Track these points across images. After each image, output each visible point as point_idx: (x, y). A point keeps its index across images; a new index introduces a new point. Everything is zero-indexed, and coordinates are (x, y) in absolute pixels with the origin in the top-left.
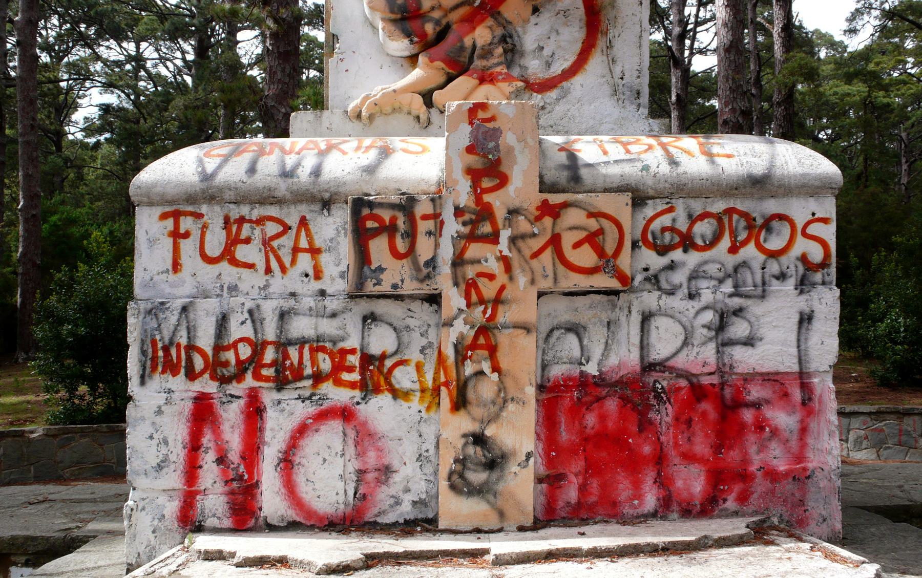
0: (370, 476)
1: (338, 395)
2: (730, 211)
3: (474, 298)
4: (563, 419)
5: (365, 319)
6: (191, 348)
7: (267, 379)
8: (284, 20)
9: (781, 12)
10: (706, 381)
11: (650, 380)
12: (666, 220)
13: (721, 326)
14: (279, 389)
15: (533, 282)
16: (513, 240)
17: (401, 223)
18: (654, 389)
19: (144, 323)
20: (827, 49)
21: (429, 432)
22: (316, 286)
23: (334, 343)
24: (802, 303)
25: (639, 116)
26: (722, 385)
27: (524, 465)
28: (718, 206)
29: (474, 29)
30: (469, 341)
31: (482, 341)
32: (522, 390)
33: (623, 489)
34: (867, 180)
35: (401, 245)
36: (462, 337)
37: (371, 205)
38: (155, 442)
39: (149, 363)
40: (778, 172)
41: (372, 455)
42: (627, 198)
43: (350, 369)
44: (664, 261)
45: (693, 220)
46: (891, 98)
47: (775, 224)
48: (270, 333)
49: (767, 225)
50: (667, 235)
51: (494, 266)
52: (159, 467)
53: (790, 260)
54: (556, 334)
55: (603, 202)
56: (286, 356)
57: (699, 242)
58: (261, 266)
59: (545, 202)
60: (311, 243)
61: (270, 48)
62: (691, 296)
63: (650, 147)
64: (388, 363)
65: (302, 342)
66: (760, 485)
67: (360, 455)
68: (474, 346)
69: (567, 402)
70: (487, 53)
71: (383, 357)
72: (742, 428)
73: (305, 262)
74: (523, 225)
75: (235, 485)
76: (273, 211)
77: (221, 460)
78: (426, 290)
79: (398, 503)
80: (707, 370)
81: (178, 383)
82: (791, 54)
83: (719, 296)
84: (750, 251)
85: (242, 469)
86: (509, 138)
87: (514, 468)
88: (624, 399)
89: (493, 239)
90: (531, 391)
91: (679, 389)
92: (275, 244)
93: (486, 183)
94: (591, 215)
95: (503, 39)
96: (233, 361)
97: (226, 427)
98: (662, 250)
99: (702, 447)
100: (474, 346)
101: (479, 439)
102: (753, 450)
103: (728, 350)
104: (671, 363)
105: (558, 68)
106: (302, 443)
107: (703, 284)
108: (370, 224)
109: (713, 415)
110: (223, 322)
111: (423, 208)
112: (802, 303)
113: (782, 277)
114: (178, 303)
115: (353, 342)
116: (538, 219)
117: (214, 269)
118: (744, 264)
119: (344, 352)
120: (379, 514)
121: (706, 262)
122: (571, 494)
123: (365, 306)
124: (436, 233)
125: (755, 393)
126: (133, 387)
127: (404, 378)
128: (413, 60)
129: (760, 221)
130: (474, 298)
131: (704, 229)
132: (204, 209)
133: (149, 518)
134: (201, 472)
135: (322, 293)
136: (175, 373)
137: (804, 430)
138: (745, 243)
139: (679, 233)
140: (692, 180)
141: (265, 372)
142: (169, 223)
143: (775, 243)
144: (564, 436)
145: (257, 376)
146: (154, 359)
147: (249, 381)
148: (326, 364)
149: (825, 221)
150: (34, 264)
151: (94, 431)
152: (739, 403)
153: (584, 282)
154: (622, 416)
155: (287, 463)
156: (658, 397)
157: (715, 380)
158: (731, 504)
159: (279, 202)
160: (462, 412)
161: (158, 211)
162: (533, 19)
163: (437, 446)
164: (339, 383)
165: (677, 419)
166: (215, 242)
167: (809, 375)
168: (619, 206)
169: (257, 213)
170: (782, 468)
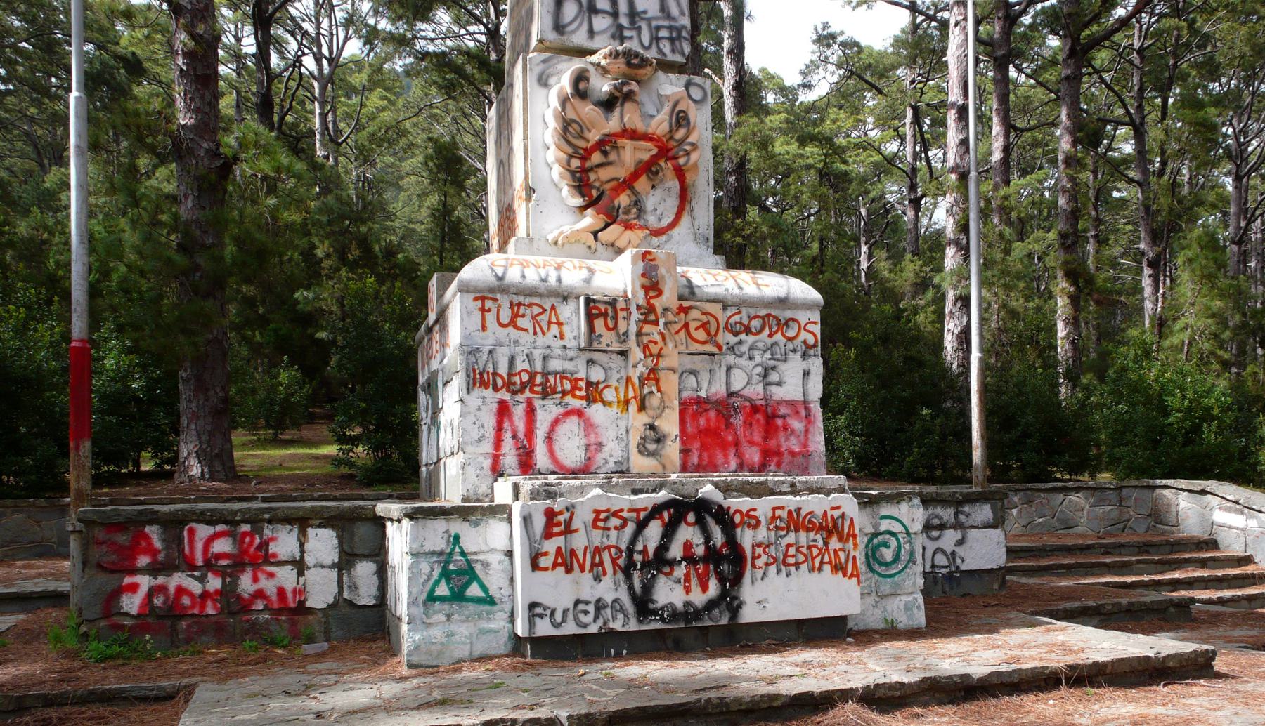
0: (593, 448)
2: (768, 315)
3: (648, 353)
4: (688, 420)
5: (588, 362)
6: (495, 374)
7: (537, 393)
8: (201, 36)
9: (733, 66)
10: (759, 403)
11: (731, 401)
12: (737, 318)
13: (765, 376)
14: (543, 399)
15: (676, 346)
16: (666, 324)
17: (610, 311)
18: (733, 406)
19: (467, 359)
20: (776, 94)
21: (622, 424)
22: (561, 343)
23: (572, 374)
24: (804, 365)
26: (767, 405)
27: (674, 441)
28: (763, 312)
29: (619, 195)
30: (645, 376)
31: (652, 376)
32: (672, 402)
33: (719, 458)
34: (822, 265)
35: (611, 324)
36: (642, 374)
37: (594, 301)
38: (476, 426)
39: (471, 382)
40: (792, 296)
41: (592, 436)
42: (720, 305)
43: (580, 389)
44: (736, 339)
45: (751, 318)
46: (848, 165)
47: (791, 323)
48: (539, 368)
49: (787, 323)
50: (738, 326)
51: (657, 337)
52: (479, 440)
54: (685, 375)
55: (709, 307)
56: (548, 381)
57: (754, 331)
58: (531, 330)
59: (681, 305)
60: (557, 319)
61: (184, 68)
62: (750, 359)
63: (727, 278)
64: (601, 386)
65: (556, 373)
66: (787, 459)
67: (587, 436)
68: (648, 379)
69: (690, 412)
71: (598, 383)
72: (777, 427)
73: (555, 329)
74: (670, 317)
75: (522, 450)
76: (536, 300)
77: (514, 437)
78: (623, 348)
79: (607, 462)
80: (759, 397)
81: (489, 393)
82: (744, 117)
83: (764, 359)
84: (778, 337)
85: (525, 442)
87: (669, 443)
88: (719, 412)
89: (656, 323)
90: (676, 403)
91: (746, 407)
92: (538, 318)
93: (652, 294)
94: (704, 313)
95: (637, 203)
96: (519, 382)
97: (516, 418)
98: (736, 334)
99: (757, 437)
100: (648, 379)
101: (652, 427)
102: (782, 440)
103: (769, 387)
104: (741, 393)
106: (557, 428)
107: (756, 352)
108: (594, 311)
109: (762, 421)
110: (512, 360)
111: (621, 305)
112: (804, 365)
113: (794, 351)
114: (487, 349)
115: (582, 374)
116: (678, 314)
117: (506, 331)
118: (775, 343)
119: (577, 380)
120: (597, 468)
121: (757, 341)
122: (694, 459)
123: (588, 355)
124: (628, 318)
127: (609, 395)
128: (583, 209)
129: (783, 321)
130: (648, 353)
131: (756, 324)
132: (498, 296)
133: (473, 469)
134: (503, 444)
135: (565, 347)
136: (487, 388)
137: (807, 431)
138: (776, 332)
139: (744, 325)
140: (750, 298)
141: (536, 389)
142: (479, 303)
143: (791, 333)
144: (689, 429)
145: (532, 391)
146: (475, 379)
147: (527, 394)
148: (568, 386)
149: (815, 323)
151: (30, 506)
153: (701, 348)
154: (717, 420)
155: (549, 439)
156: (735, 410)
157: (763, 403)
158: (773, 467)
159: (540, 295)
160: (643, 413)
161: (472, 296)
162: (652, 192)
163: (627, 431)
164: (574, 396)
165: (745, 422)
166: (505, 316)
167: (809, 403)
168: (715, 309)
169: (528, 301)
170: (797, 449)
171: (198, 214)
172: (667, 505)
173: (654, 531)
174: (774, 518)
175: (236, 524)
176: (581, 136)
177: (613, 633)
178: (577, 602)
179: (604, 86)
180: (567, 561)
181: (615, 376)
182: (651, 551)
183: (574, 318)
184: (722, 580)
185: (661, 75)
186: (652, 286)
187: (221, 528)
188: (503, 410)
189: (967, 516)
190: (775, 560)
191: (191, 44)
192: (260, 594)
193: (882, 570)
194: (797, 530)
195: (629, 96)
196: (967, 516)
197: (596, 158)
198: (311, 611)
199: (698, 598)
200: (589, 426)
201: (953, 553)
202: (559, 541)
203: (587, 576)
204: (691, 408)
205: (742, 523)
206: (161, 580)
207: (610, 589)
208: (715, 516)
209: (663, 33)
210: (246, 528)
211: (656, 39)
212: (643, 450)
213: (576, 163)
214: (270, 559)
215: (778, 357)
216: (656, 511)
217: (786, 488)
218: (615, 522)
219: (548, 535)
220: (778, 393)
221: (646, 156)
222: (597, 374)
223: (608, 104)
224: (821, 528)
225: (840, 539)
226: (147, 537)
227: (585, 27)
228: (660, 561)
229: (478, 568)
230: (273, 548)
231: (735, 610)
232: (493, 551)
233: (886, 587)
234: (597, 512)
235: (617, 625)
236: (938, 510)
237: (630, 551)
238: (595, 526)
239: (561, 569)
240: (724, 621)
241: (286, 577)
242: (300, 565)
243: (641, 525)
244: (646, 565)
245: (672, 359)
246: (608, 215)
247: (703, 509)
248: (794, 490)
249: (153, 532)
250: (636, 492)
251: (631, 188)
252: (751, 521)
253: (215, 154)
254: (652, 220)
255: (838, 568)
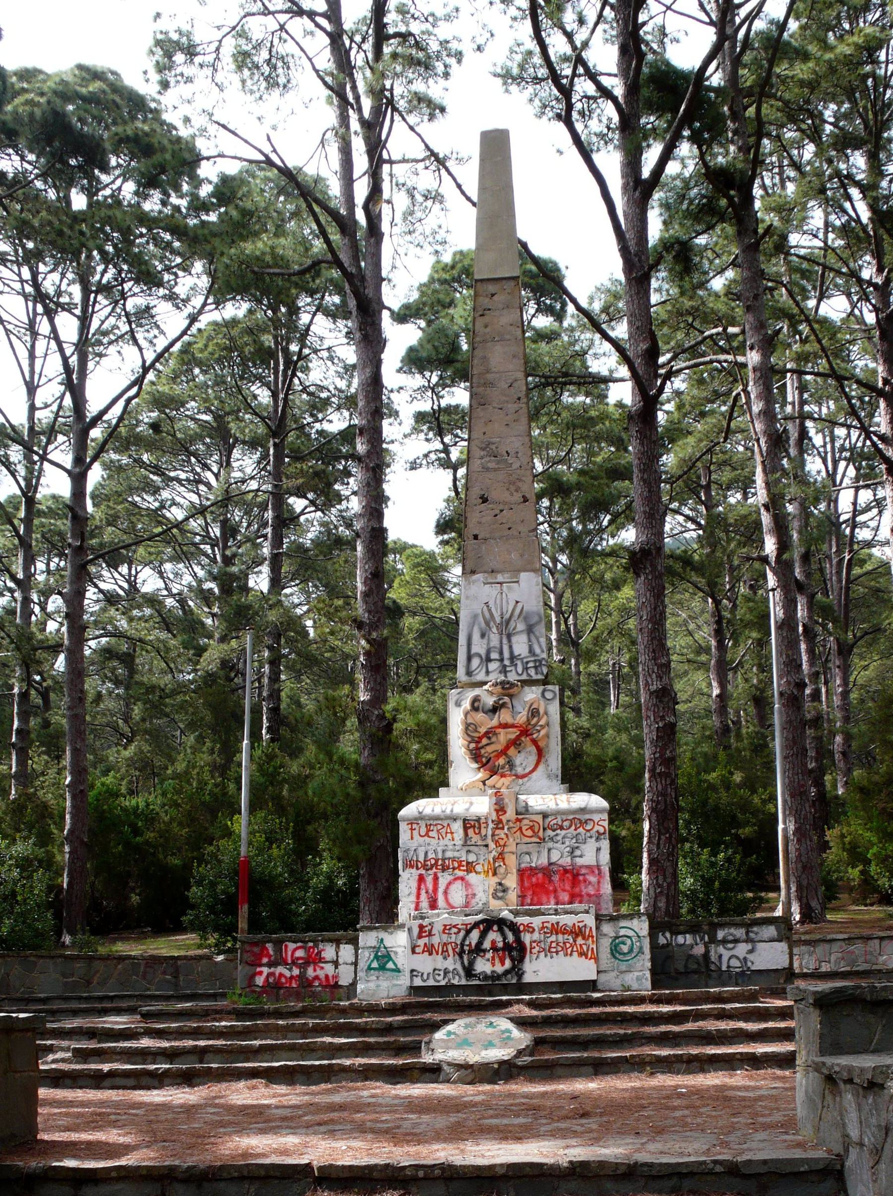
1: (459, 873)
21: (486, 883)
24: (597, 845)
25: (557, 785)
28: (571, 817)
49: (586, 822)
51: (503, 836)
53: (593, 832)
55: (534, 817)
66: (586, 898)
70: (503, 767)
73: (449, 836)
74: (511, 824)
77: (427, 892)
81: (414, 871)
84: (581, 830)
86: (506, 800)
89: (503, 828)
90: (515, 871)
98: (554, 830)
99: (568, 887)
101: (500, 884)
105: (527, 771)
110: (426, 853)
112: (597, 845)
115: (464, 858)
123: (467, 848)
124: (487, 827)
125: (583, 871)
126: (401, 872)
127: (479, 868)
128: (479, 769)
131: (566, 824)
137: (599, 882)
143: (588, 827)
144: (526, 884)
147: (434, 870)
148: (456, 865)
150: (82, 842)
152: (578, 874)
153: (529, 840)
155: (446, 893)
166: (423, 831)
171: (371, 760)
172: (482, 921)
173: (475, 935)
174: (543, 928)
175: (305, 942)
176: (476, 731)
177: (453, 985)
178: (435, 970)
179: (490, 701)
180: (429, 950)
181: (482, 858)
182: (473, 945)
183: (457, 827)
184: (512, 959)
185: (526, 688)
186: (500, 809)
187: (299, 944)
188: (421, 879)
189: (756, 934)
190: (544, 950)
191: (367, 646)
192: (317, 978)
193: (620, 957)
194: (557, 934)
195: (503, 705)
196: (756, 934)
197: (485, 741)
198: (341, 987)
199: (499, 969)
200: (468, 885)
201: (745, 959)
202: (426, 940)
203: (440, 957)
204: (523, 874)
205: (524, 930)
206: (272, 970)
207: (451, 963)
208: (508, 927)
209: (531, 664)
210: (311, 944)
211: (526, 669)
212: (495, 896)
213: (473, 745)
214: (321, 960)
215: (580, 841)
216: (476, 925)
217: (551, 912)
218: (454, 930)
219: (420, 937)
220: (579, 861)
221: (513, 736)
222: (472, 858)
223: (495, 710)
224: (571, 932)
225: (584, 938)
226: (267, 949)
227: (484, 670)
228: (478, 950)
229: (392, 955)
230: (323, 955)
231: (520, 975)
232: (400, 946)
233: (623, 967)
234: (445, 926)
235: (455, 982)
236: (732, 930)
237: (462, 945)
238: (444, 932)
239: (426, 954)
240: (514, 981)
241: (329, 969)
242: (336, 964)
243: (468, 932)
244: (471, 952)
245: (512, 847)
246: (491, 771)
247: (501, 923)
248: (556, 913)
249: (269, 946)
250: (466, 915)
251: (506, 754)
252: (530, 929)
253: (382, 717)
254: (520, 770)
255: (582, 954)
